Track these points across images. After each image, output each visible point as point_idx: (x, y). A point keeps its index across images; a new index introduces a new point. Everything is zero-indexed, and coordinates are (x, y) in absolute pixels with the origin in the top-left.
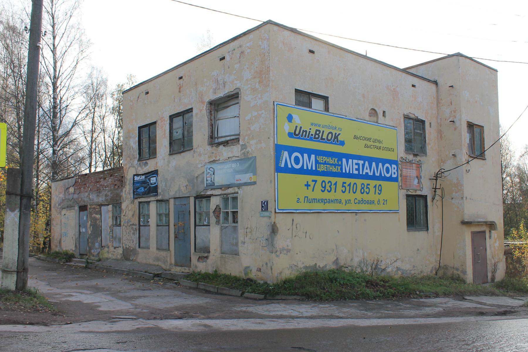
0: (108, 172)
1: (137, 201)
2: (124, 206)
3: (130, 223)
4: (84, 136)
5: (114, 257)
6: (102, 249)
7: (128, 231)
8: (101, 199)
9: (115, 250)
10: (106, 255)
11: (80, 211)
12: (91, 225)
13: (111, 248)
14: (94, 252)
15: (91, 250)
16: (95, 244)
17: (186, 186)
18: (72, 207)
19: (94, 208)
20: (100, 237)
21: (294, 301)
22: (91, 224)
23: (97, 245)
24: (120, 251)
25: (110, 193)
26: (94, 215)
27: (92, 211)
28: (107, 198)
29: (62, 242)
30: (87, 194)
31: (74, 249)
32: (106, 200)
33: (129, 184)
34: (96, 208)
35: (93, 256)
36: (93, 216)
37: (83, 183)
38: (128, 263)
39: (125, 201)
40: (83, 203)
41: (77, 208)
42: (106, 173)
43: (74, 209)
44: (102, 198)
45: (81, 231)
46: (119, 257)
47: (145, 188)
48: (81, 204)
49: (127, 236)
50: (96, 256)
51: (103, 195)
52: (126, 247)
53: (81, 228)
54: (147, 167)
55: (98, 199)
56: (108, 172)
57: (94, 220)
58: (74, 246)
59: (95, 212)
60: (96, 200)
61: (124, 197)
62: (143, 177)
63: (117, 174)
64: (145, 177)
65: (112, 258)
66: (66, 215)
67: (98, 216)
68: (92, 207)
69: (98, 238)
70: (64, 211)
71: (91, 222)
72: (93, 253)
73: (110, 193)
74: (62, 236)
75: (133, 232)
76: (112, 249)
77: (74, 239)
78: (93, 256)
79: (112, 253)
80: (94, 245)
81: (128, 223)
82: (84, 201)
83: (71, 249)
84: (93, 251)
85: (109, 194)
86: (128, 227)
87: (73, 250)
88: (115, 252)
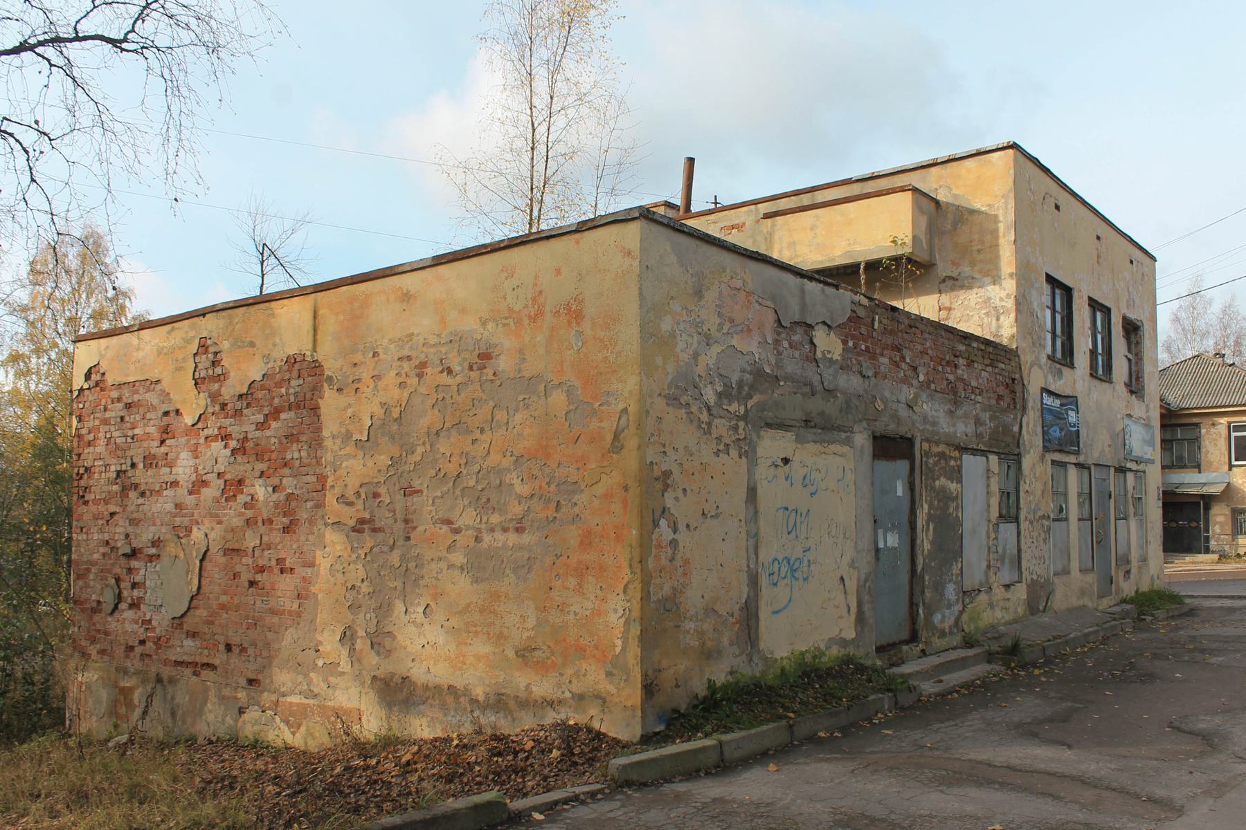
0: (983, 347)
1: (1050, 456)
2: (1027, 463)
3: (1040, 513)
4: (12, 68)
5: (1008, 617)
6: (967, 600)
7: (1035, 534)
8: (962, 429)
9: (1009, 595)
10: (987, 618)
11: (873, 460)
12: (930, 518)
13: (998, 590)
14: (942, 621)
15: (932, 615)
16: (944, 588)
17: (1110, 446)
18: (840, 429)
19: (942, 455)
20: (957, 562)
21: (711, 785)
22: (929, 513)
23: (950, 591)
24: (1021, 592)
25: (988, 414)
26: (943, 479)
27: (935, 464)
28: (980, 429)
29: (764, 614)
30: (907, 393)
31: (850, 634)
32: (979, 436)
33: (1033, 408)
34: (951, 457)
35: (943, 634)
36: (937, 483)
37: (889, 340)
38: (1045, 619)
39: (1029, 452)
40: (892, 427)
41: (862, 439)
42: (975, 345)
43: (848, 442)
44: (966, 427)
45: (881, 545)
46: (1020, 610)
47: (1061, 429)
48: (880, 427)
49: (1033, 548)
50: (951, 633)
51: (966, 416)
52: (1032, 579)
53: (880, 532)
54: (1062, 382)
55: (954, 425)
56: (983, 347)
57: (939, 501)
58: (853, 617)
59: (943, 468)
60: (945, 426)
61: (1025, 439)
62: (1058, 402)
63: (1003, 366)
64: (1062, 405)
65: (1003, 621)
66: (795, 464)
67: (953, 486)
68: (936, 449)
69: (952, 565)
70: (772, 445)
71: (930, 507)
72: (939, 626)
73: (988, 414)
74: (764, 581)
75: (1043, 536)
76: (999, 592)
77: (852, 585)
78: (943, 634)
79: (1001, 604)
80: (942, 594)
81: (1035, 513)
82: (896, 418)
83: (831, 641)
84: (937, 618)
85: (986, 416)
86: (1035, 523)
87: (844, 643)
88: (1008, 599)
